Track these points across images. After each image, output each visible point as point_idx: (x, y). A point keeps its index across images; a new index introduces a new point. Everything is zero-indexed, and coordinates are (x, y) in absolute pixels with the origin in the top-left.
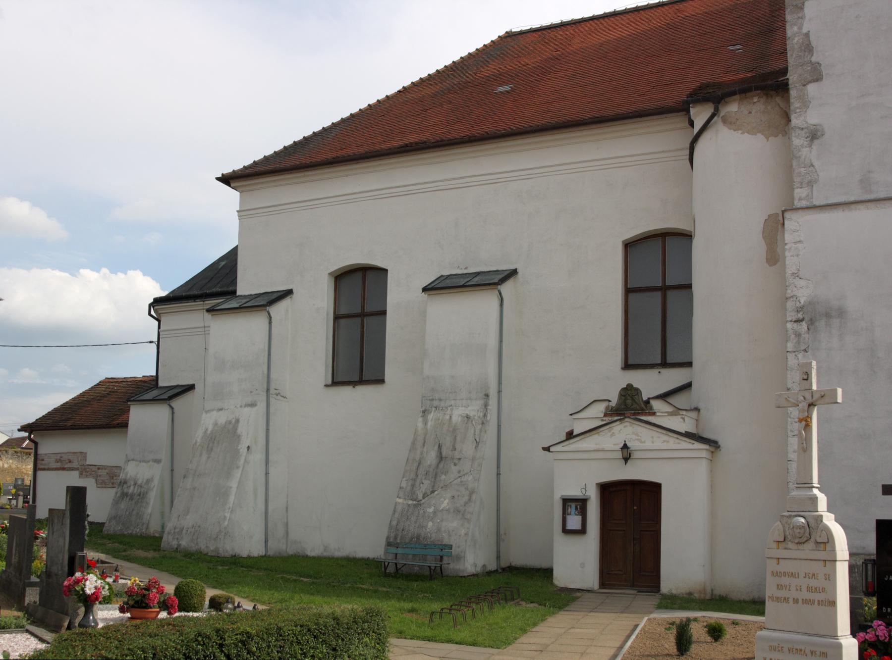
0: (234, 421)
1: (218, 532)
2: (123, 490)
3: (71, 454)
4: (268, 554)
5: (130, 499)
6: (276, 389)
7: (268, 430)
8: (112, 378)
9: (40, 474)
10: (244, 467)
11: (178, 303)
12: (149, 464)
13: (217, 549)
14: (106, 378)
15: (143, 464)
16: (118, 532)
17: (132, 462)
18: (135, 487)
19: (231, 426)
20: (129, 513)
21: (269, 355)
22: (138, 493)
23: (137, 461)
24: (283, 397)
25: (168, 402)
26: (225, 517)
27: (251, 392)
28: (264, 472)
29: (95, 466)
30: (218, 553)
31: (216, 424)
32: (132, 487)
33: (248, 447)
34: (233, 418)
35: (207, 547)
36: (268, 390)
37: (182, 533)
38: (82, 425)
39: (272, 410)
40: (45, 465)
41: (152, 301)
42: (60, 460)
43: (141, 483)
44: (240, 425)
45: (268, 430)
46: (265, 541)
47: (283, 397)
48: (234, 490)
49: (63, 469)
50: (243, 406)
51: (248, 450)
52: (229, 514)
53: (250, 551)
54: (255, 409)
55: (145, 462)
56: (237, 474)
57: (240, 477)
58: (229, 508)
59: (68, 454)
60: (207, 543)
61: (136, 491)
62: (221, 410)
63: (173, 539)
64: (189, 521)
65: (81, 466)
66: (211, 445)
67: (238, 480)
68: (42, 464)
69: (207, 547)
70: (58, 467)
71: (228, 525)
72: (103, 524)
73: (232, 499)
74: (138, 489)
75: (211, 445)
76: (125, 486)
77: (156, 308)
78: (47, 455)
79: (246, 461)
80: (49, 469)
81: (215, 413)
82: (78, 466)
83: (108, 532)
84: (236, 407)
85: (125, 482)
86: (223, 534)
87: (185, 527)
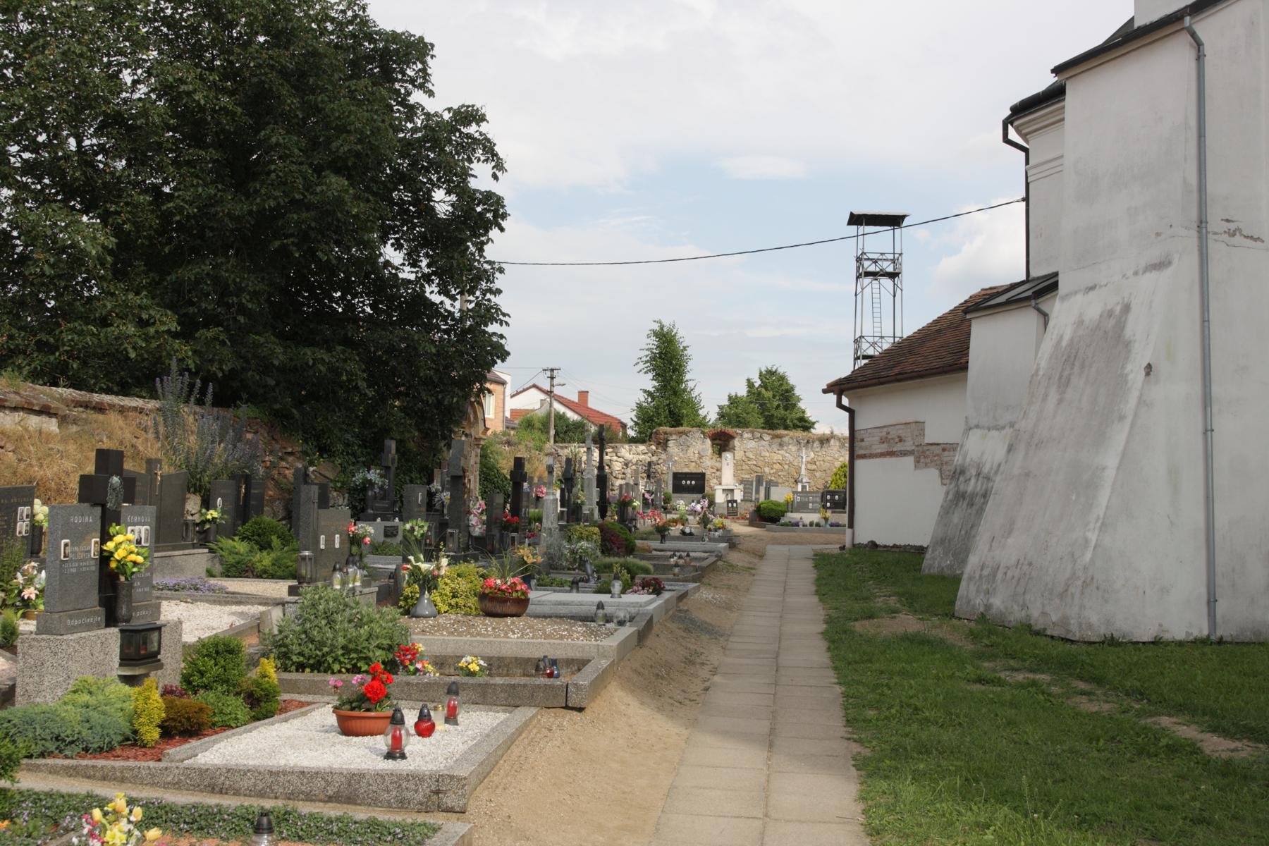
0: (1118, 309)
1: (1068, 579)
2: (958, 488)
3: (902, 427)
4: (1219, 633)
5: (968, 505)
6: (1228, 221)
7: (1205, 321)
8: (991, 289)
9: (859, 463)
10: (1136, 415)
11: (1053, 104)
12: (1004, 432)
13: (1065, 621)
14: (982, 290)
15: (994, 433)
16: (945, 569)
17: (975, 430)
18: (978, 480)
19: (1112, 322)
20: (967, 532)
21: (1201, 135)
22: (983, 491)
23: (983, 428)
24: (1251, 238)
25: (1033, 303)
26: (1087, 541)
27: (1158, 234)
28: (1200, 428)
29: (938, 444)
30: (1068, 631)
31: (1080, 323)
32: (973, 481)
33: (1149, 367)
34: (1118, 304)
35: (1044, 614)
36: (1202, 223)
37: (995, 576)
38: (912, 372)
39: (1215, 272)
40: (866, 448)
41: (1009, 113)
42: (887, 438)
43: (989, 472)
44: (1132, 317)
45: (1205, 321)
46: (1209, 602)
47: (1251, 238)
48: (1110, 474)
49: (891, 454)
50: (1141, 272)
51: (1148, 374)
52: (1096, 532)
53: (1161, 625)
54: (1169, 272)
55: (998, 429)
56: (1119, 435)
57: (1127, 442)
58: (1098, 519)
59: (897, 427)
60: (1043, 606)
61: (978, 488)
62: (1092, 288)
63: (978, 591)
64: (1010, 551)
65: (917, 446)
66: (1066, 373)
67: (1120, 449)
68: (861, 448)
69: (1044, 614)
70: (884, 451)
71: (1092, 560)
72: (921, 550)
73: (1104, 496)
74: (982, 484)
75: (1066, 373)
76: (961, 479)
77: (1016, 123)
78: (869, 431)
79: (1141, 401)
80: (872, 456)
81: (1079, 297)
82: (913, 448)
83: (929, 570)
84: (1124, 276)
85: (962, 472)
86: (1079, 583)
87: (1002, 565)
